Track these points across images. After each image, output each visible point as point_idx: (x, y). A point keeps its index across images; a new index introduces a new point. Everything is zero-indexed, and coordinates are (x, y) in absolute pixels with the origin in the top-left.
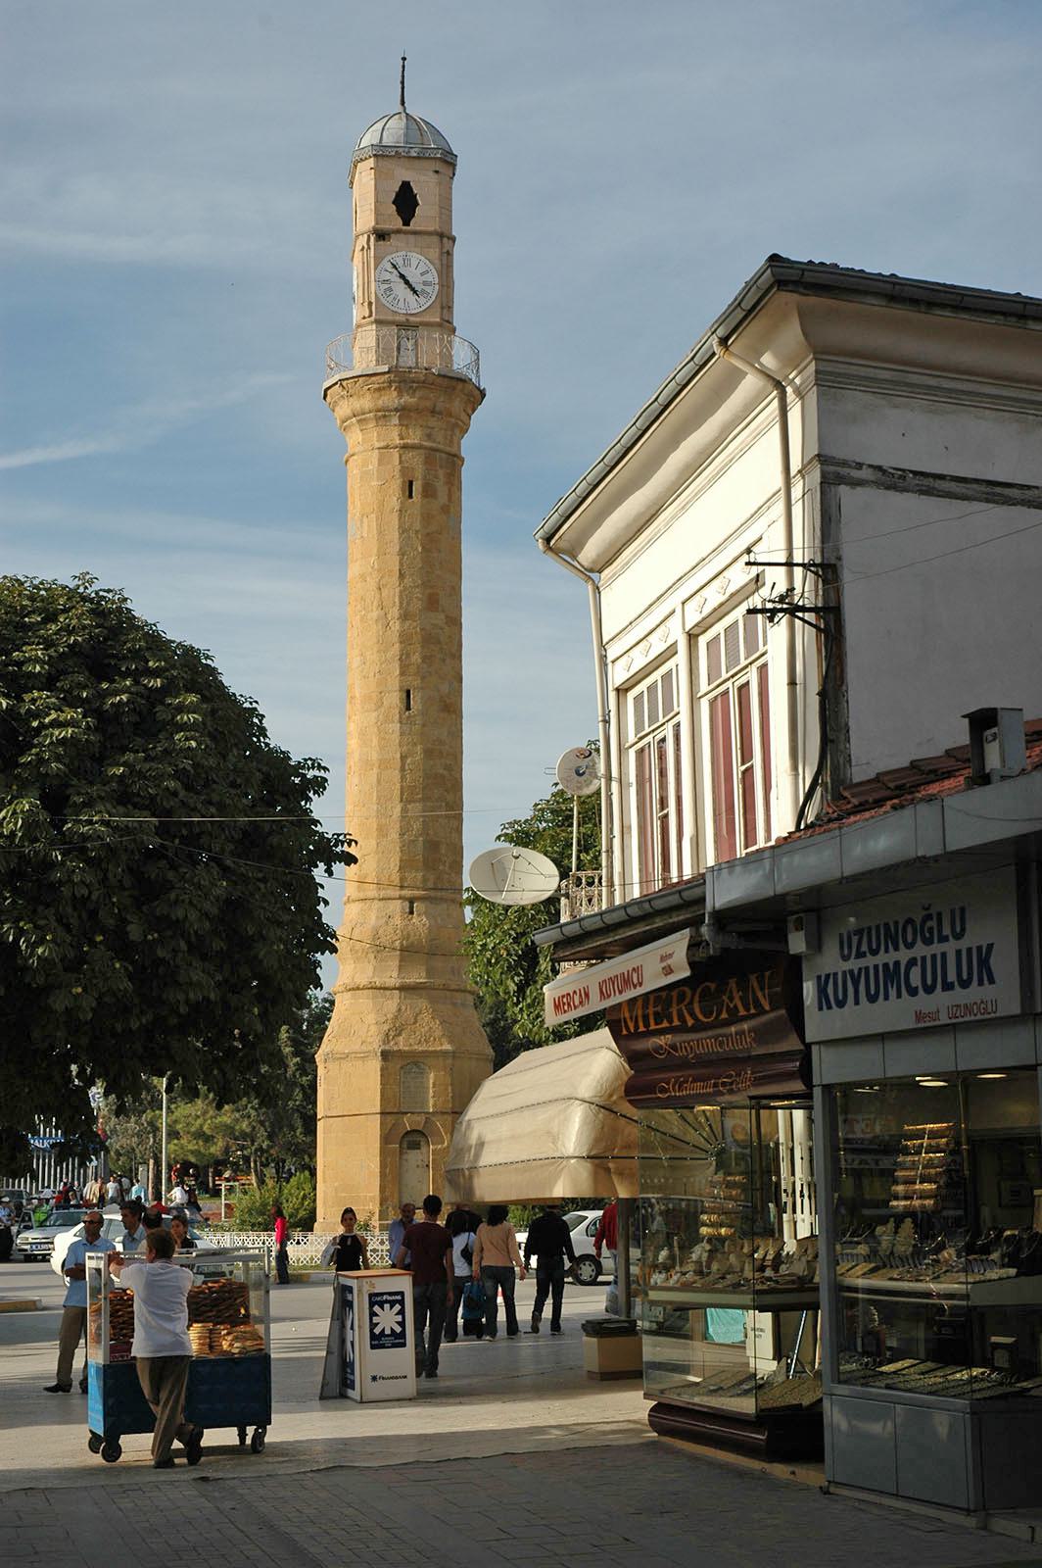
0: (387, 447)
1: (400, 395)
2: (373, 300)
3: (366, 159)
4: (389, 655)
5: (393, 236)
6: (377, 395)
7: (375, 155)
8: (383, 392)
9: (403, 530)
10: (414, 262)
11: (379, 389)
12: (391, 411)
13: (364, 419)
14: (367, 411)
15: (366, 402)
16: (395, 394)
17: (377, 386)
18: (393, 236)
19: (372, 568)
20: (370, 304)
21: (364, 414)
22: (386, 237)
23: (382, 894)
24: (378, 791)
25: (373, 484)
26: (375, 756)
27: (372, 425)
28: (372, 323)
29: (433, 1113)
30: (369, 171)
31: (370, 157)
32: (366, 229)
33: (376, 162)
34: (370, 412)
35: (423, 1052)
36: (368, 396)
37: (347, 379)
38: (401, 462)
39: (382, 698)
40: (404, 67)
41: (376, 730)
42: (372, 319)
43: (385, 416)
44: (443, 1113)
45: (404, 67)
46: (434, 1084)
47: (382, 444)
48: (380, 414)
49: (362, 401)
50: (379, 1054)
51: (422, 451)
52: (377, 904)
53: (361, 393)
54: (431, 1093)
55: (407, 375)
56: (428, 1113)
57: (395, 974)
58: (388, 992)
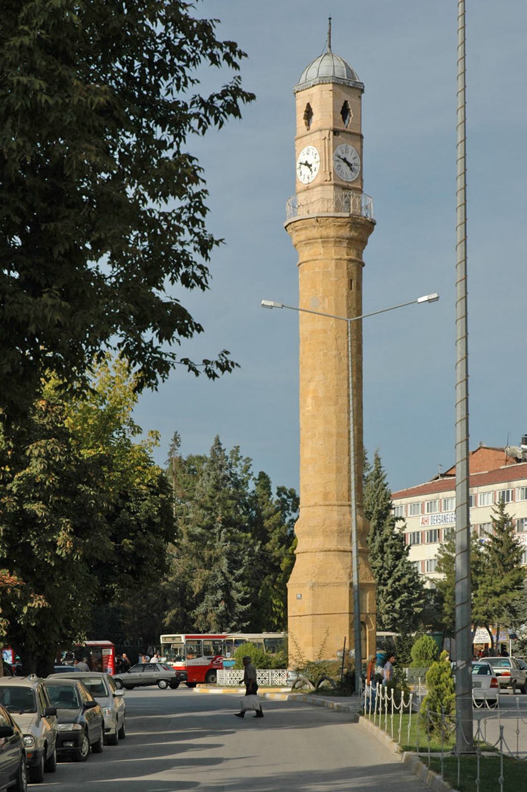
0: (340, 259)
1: (351, 230)
2: (332, 171)
3: (326, 83)
4: (342, 376)
5: (340, 133)
6: (338, 228)
7: (333, 83)
8: (342, 228)
9: (349, 308)
10: (350, 151)
11: (340, 226)
12: (344, 239)
13: (327, 241)
14: (331, 236)
15: (332, 232)
16: (348, 229)
17: (339, 224)
18: (340, 133)
19: (332, 327)
20: (330, 173)
21: (328, 238)
22: (337, 133)
23: (340, 503)
24: (336, 449)
25: (331, 279)
26: (334, 431)
27: (330, 245)
28: (331, 185)
29: (369, 614)
30: (329, 92)
31: (329, 83)
32: (328, 127)
33: (333, 87)
34: (333, 238)
35: (366, 584)
36: (333, 229)
37: (322, 217)
38: (347, 269)
39: (337, 400)
40: (330, 24)
41: (334, 416)
42: (332, 182)
43: (340, 241)
44: (373, 614)
45: (330, 24)
46: (369, 599)
47: (339, 257)
48: (338, 240)
49: (328, 231)
50: (348, 584)
51: (356, 263)
52: (335, 508)
53: (329, 226)
54: (368, 605)
55: (357, 220)
56: (366, 613)
57: (335, 543)
58: (345, 553)
